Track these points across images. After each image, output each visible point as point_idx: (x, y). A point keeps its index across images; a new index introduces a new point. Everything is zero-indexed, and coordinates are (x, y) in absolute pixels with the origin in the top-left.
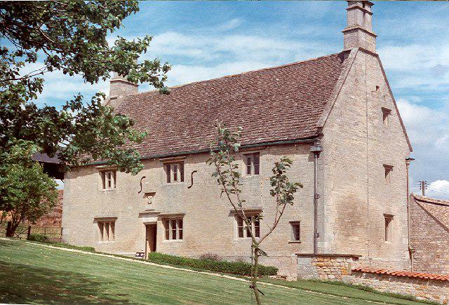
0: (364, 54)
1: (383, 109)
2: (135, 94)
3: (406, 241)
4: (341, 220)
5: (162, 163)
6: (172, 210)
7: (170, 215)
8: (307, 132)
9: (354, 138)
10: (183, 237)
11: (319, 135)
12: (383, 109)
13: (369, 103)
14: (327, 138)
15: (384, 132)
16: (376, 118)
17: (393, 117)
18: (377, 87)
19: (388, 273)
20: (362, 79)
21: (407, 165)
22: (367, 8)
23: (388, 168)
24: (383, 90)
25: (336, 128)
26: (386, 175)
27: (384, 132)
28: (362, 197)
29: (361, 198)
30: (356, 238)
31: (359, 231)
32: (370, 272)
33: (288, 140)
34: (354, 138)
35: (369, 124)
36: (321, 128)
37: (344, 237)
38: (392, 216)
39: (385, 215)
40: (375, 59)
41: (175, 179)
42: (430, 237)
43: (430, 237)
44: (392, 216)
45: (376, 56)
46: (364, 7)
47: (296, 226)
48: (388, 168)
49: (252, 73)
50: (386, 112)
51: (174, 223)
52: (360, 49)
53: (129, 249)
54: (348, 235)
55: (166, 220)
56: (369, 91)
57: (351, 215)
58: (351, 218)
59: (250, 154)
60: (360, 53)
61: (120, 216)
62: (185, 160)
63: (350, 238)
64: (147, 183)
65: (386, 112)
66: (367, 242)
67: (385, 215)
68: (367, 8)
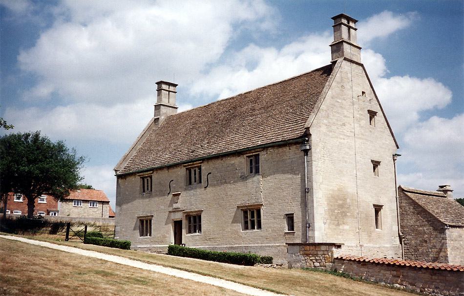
0: (349, 63)
1: (369, 111)
2: (174, 114)
3: (395, 228)
4: (331, 211)
5: (185, 168)
6: (194, 208)
7: (192, 212)
8: (299, 133)
9: (341, 137)
10: (262, 226)
11: (307, 135)
12: (369, 111)
13: (356, 106)
14: (314, 138)
15: (370, 131)
16: (363, 119)
17: (379, 118)
18: (363, 93)
19: (367, 260)
20: (348, 86)
21: (394, 160)
22: (352, 24)
23: (376, 164)
24: (369, 94)
25: (323, 129)
26: (374, 169)
27: (370, 131)
28: (351, 189)
29: (349, 190)
30: (346, 227)
31: (349, 220)
32: (350, 260)
33: (282, 141)
34: (341, 137)
35: (356, 125)
36: (308, 129)
37: (335, 227)
38: (381, 206)
39: (374, 205)
40: (361, 68)
41: (195, 182)
42: (418, 223)
43: (418, 223)
44: (381, 206)
45: (362, 65)
46: (348, 23)
47: (290, 218)
48: (376, 164)
49: (259, 89)
50: (372, 114)
51: (194, 222)
52: (345, 59)
53: (162, 242)
54: (338, 225)
55: (188, 216)
56: (355, 96)
57: (341, 206)
58: (341, 208)
59: (251, 156)
60: (345, 62)
61: (155, 214)
62: (202, 165)
63: (341, 227)
64: (174, 185)
65: (372, 114)
66: (358, 230)
67: (374, 205)
68: (352, 24)
